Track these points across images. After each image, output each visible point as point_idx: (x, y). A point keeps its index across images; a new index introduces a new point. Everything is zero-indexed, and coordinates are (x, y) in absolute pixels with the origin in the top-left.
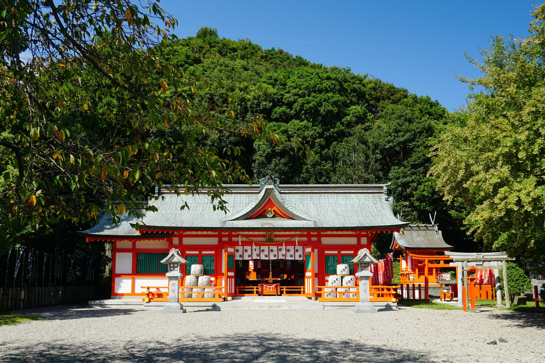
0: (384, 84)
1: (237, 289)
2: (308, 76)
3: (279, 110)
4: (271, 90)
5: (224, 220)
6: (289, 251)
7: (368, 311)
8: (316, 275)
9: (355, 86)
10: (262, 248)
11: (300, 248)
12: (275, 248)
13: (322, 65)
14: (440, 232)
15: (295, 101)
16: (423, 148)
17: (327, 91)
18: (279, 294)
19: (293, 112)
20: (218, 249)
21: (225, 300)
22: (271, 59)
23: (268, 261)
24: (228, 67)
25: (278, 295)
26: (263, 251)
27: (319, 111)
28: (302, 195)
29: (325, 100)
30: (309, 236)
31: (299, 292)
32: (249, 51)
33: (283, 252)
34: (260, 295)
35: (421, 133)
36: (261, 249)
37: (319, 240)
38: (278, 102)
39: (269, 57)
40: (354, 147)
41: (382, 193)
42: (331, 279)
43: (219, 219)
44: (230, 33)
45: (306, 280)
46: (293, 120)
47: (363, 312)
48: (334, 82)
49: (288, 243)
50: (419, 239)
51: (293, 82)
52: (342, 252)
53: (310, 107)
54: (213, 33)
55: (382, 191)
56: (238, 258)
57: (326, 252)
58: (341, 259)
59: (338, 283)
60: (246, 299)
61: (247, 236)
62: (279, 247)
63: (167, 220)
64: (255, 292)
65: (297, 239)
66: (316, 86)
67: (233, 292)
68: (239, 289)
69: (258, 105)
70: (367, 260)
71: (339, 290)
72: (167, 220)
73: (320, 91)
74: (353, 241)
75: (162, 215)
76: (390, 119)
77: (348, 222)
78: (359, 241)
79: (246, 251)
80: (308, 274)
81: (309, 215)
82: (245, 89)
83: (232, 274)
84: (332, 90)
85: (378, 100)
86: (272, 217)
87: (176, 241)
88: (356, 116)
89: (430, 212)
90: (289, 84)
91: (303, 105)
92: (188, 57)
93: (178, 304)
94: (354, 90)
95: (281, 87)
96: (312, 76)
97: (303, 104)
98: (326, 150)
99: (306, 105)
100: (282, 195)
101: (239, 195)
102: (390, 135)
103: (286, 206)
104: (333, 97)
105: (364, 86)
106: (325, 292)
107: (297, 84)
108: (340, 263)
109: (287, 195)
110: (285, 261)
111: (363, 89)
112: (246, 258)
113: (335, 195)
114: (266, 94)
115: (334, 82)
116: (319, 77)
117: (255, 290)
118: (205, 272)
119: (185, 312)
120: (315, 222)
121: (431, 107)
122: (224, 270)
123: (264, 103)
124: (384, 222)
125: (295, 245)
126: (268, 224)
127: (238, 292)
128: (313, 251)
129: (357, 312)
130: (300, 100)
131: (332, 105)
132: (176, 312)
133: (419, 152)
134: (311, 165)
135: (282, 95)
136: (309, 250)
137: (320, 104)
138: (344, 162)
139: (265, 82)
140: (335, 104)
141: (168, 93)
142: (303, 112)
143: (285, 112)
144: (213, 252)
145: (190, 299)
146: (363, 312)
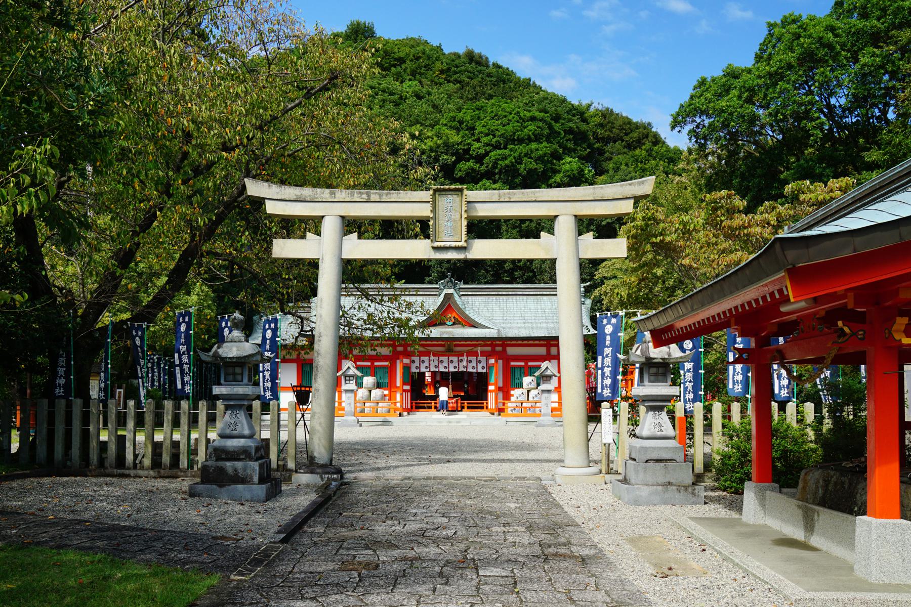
2: (505, 116)
3: (464, 166)
4: (455, 138)
6: (470, 362)
7: (548, 426)
9: (571, 124)
10: (441, 358)
11: (483, 359)
12: (455, 359)
13: (530, 80)
15: (487, 154)
17: (530, 140)
19: (483, 167)
20: (393, 358)
21: (400, 415)
22: (455, 73)
23: (448, 373)
26: (442, 362)
27: (518, 169)
28: (487, 297)
29: (526, 155)
30: (493, 346)
31: (482, 408)
37: (504, 351)
38: (463, 155)
42: (516, 393)
46: (484, 181)
47: (543, 426)
48: (541, 124)
49: (469, 354)
51: (483, 126)
52: (530, 364)
53: (507, 166)
56: (414, 370)
57: (512, 363)
58: (529, 371)
59: (524, 398)
60: (421, 415)
65: (479, 349)
70: (351, 372)
71: (524, 405)
73: (521, 141)
78: (548, 351)
79: (423, 362)
80: (491, 388)
83: (407, 387)
84: (537, 138)
85: (606, 140)
88: (569, 176)
90: (479, 129)
91: (495, 163)
93: (354, 418)
94: (570, 131)
95: (467, 132)
96: (510, 117)
99: (500, 162)
100: (463, 298)
103: (467, 313)
104: (537, 150)
107: (489, 129)
108: (526, 376)
109: (470, 298)
111: (584, 127)
112: (423, 370)
113: (525, 297)
114: (447, 145)
115: (541, 124)
116: (520, 118)
117: (433, 405)
118: (379, 386)
119: (361, 425)
120: (499, 331)
122: (398, 384)
123: (446, 157)
125: (477, 356)
126: (447, 333)
128: (496, 361)
129: (537, 426)
131: (535, 161)
132: (353, 426)
135: (468, 144)
136: (492, 361)
137: (519, 161)
139: (445, 125)
140: (539, 159)
142: (497, 171)
143: (473, 169)
145: (362, 414)
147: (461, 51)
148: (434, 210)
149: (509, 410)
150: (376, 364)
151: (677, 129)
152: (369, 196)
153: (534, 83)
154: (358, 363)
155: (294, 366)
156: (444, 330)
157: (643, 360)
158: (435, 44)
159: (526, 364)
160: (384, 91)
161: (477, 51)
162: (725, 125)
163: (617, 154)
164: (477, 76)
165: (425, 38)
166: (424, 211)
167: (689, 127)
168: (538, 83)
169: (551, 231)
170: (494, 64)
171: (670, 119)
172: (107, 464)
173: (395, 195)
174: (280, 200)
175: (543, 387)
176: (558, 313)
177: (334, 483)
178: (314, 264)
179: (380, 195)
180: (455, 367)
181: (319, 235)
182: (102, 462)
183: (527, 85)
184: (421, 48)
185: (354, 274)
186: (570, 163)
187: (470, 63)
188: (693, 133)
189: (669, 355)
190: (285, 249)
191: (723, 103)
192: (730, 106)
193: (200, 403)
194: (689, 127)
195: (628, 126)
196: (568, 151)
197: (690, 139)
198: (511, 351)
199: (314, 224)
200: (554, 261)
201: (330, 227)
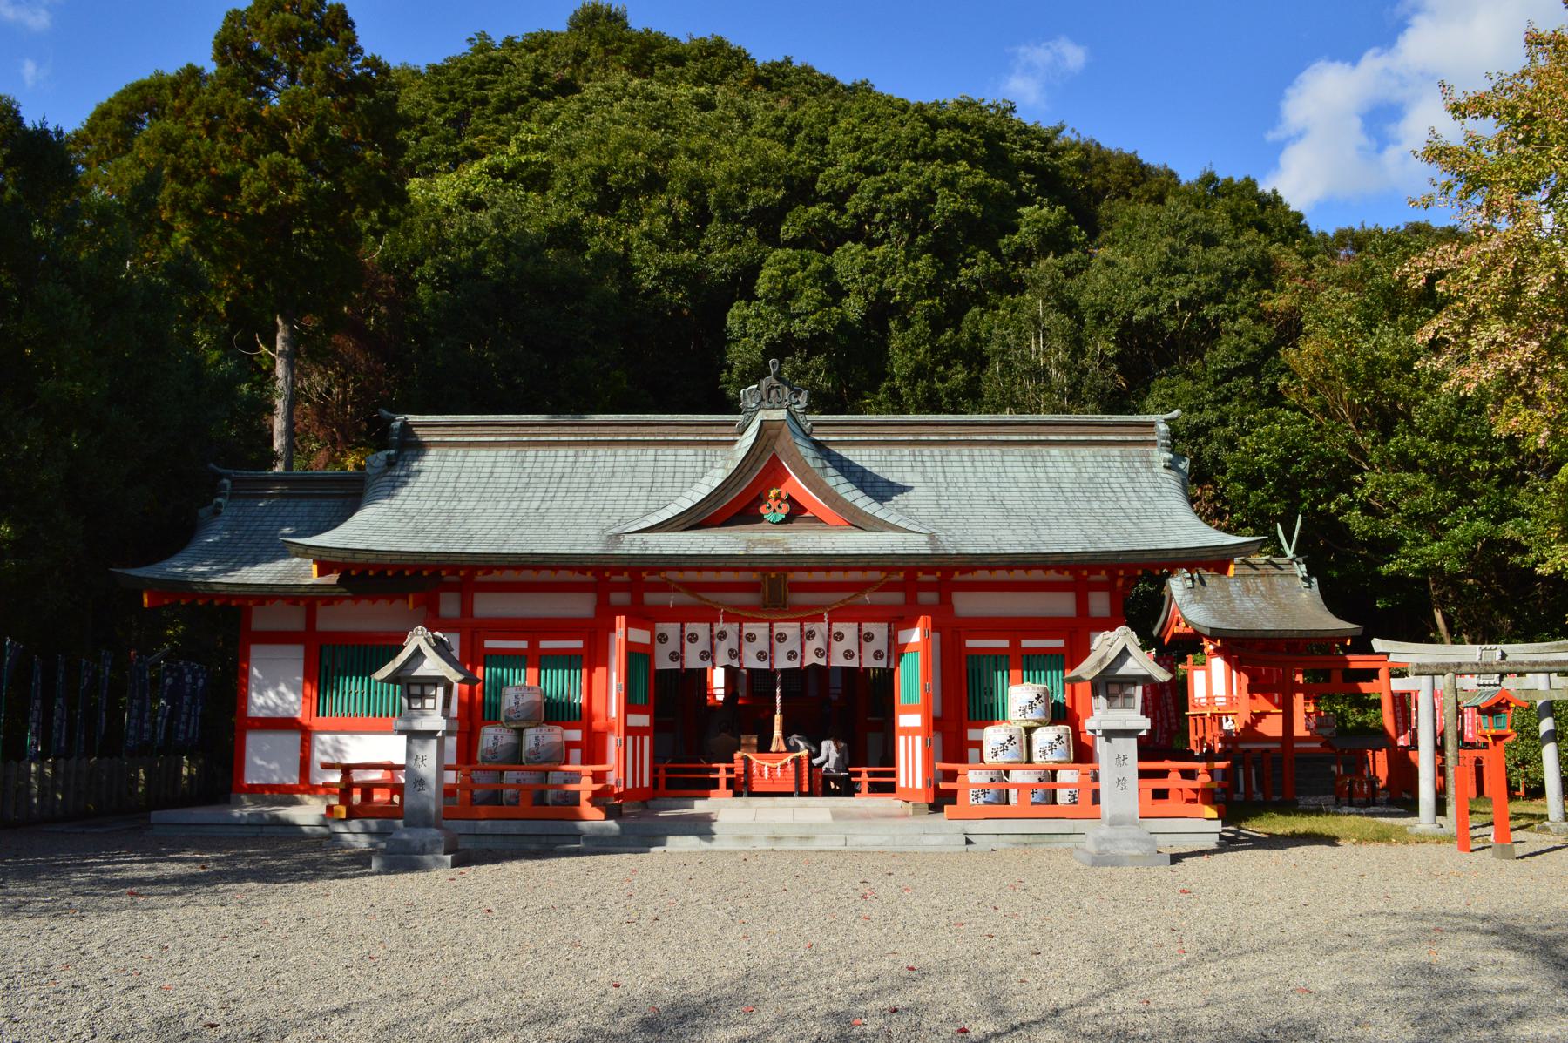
0: (1110, 153)
1: (662, 773)
5: (615, 531)
7: (1135, 860)
10: (748, 628)
12: (791, 629)
14: (1314, 580)
15: (853, 188)
16: (1249, 321)
18: (806, 789)
23: (770, 674)
24: (655, 99)
25: (802, 794)
28: (884, 450)
29: (945, 183)
32: (717, 61)
34: (737, 794)
35: (1242, 275)
36: (745, 631)
37: (946, 602)
38: (801, 190)
39: (774, 78)
40: (1035, 320)
41: (1154, 443)
42: (992, 736)
43: (598, 528)
45: (901, 741)
46: (849, 244)
47: (1116, 862)
50: (1249, 604)
52: (1026, 643)
53: (901, 203)
54: (616, 19)
55: (1150, 438)
56: (663, 663)
57: (970, 643)
61: (692, 587)
62: (808, 626)
63: (417, 531)
64: (722, 783)
66: (916, 141)
67: (646, 783)
68: (667, 771)
69: (742, 198)
70: (1132, 667)
72: (417, 531)
74: (1062, 605)
75: (405, 514)
76: (1145, 237)
77: (1045, 537)
78: (1082, 604)
80: (908, 720)
81: (909, 515)
82: (702, 155)
83: (643, 720)
86: (783, 522)
89: (1280, 519)
92: (538, 78)
98: (949, 333)
101: (669, 451)
102: (1147, 281)
105: (1054, 155)
106: (969, 786)
110: (820, 673)
112: (693, 661)
113: (996, 451)
114: (767, 166)
117: (722, 776)
120: (932, 537)
121: (1263, 206)
124: (1172, 537)
126: (767, 543)
127: (662, 782)
130: (869, 184)
133: (1239, 334)
134: (904, 378)
138: (1008, 365)
141: (618, 373)
144: (578, 644)
146: (1116, 862)
150: (544, 645)
155: (296, 653)
156: (757, 536)
159: (1015, 644)
180: (791, 655)
198: (967, 604)
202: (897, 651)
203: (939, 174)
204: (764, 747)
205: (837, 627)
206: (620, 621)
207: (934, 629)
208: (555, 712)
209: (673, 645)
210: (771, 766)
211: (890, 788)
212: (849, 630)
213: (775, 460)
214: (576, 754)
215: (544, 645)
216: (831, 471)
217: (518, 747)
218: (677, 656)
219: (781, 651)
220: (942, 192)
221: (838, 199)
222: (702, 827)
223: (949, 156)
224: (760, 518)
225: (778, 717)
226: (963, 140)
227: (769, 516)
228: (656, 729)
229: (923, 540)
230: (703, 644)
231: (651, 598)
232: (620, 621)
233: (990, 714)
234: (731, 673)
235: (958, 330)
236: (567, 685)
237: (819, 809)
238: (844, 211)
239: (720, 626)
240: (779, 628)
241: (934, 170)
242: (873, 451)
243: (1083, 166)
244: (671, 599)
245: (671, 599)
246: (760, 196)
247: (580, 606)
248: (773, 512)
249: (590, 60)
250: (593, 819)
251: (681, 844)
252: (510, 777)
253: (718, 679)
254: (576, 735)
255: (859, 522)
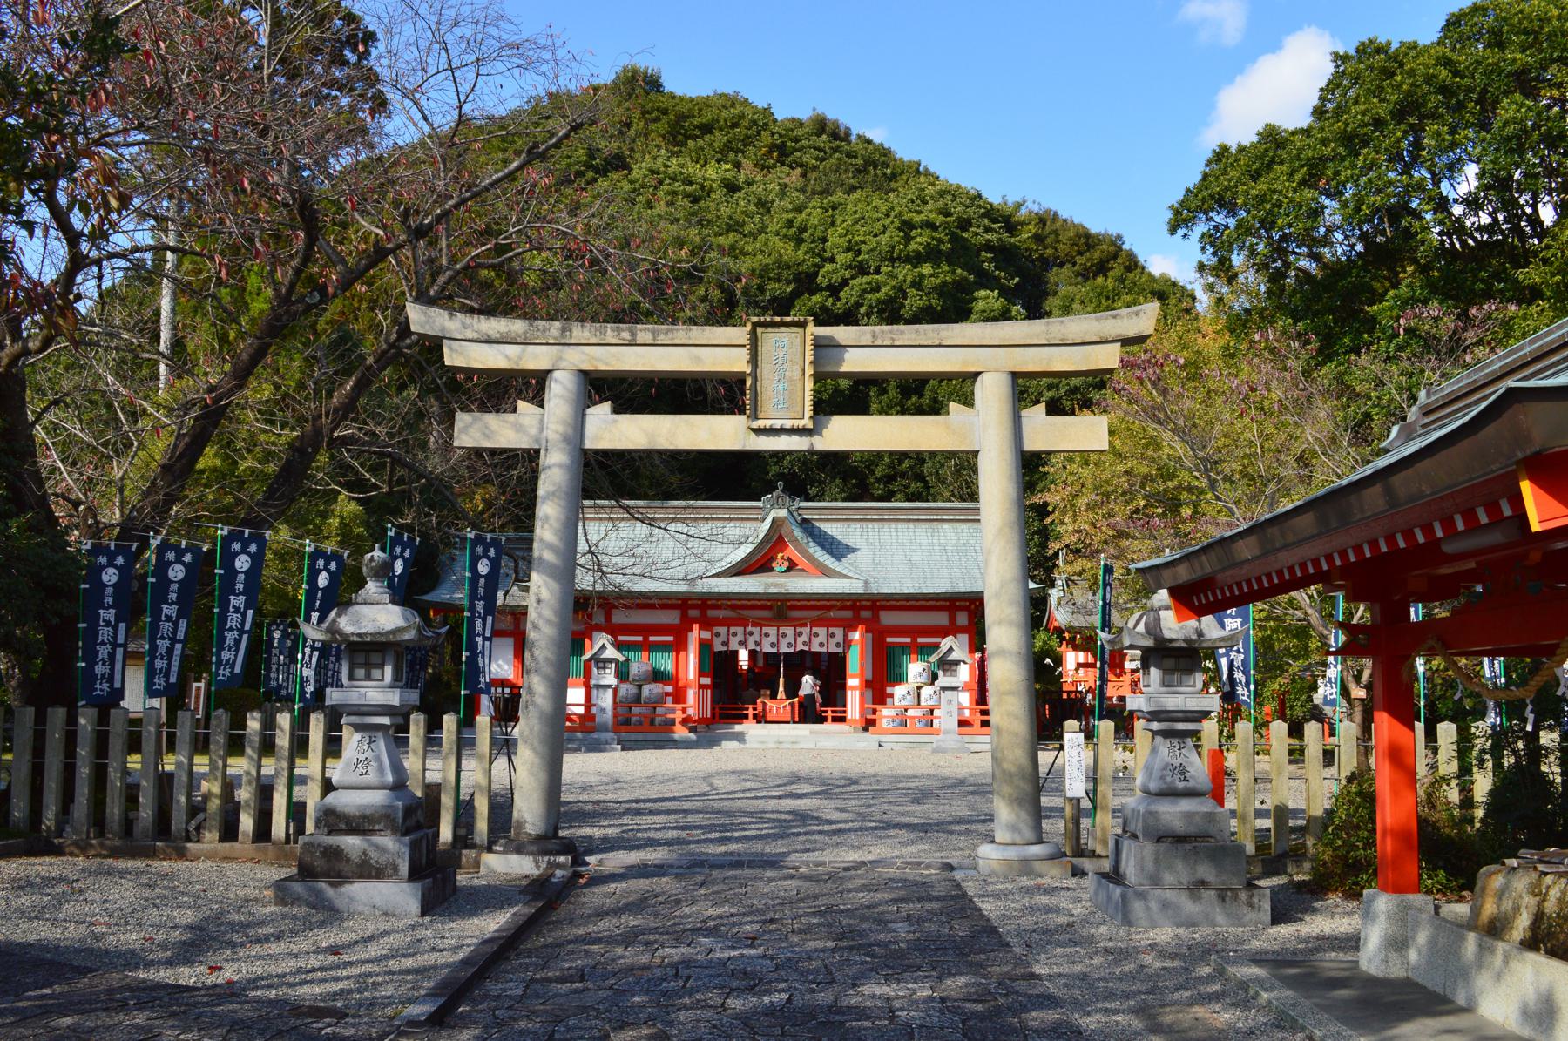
8: (867, 684)
9: (989, 236)
10: (765, 630)
12: (789, 631)
15: (845, 283)
23: (777, 655)
33: (804, 638)
37: (876, 618)
42: (899, 691)
44: (687, 80)
45: (849, 693)
52: (920, 640)
56: (718, 647)
57: (889, 640)
69: (761, 289)
78: (952, 619)
80: (853, 682)
82: (733, 251)
83: (707, 681)
87: (599, 618)
97: (864, 291)
98: (914, 398)
113: (911, 525)
114: (780, 264)
117: (750, 712)
120: (866, 582)
126: (776, 585)
144: (671, 638)
147: (804, 114)
148: (754, 359)
149: (885, 721)
151: (1181, 232)
152: (633, 335)
153: (926, 169)
154: (621, 638)
155: (510, 641)
156: (770, 580)
157: (1149, 643)
158: (761, 103)
160: (673, 179)
161: (831, 116)
162: (1268, 224)
163: (1062, 280)
164: (833, 156)
165: (745, 93)
166: (736, 361)
167: (1201, 228)
168: (932, 169)
169: (968, 401)
170: (859, 136)
171: (1169, 215)
172: (138, 829)
173: (681, 334)
174: (476, 344)
175: (943, 681)
176: (970, 550)
177: (559, 873)
178: (530, 458)
179: (654, 332)
180: (789, 645)
181: (541, 406)
182: (128, 826)
183: (915, 170)
184: (739, 109)
185: (611, 478)
186: (987, 299)
187: (819, 135)
188: (1208, 240)
189: (1200, 634)
190: (477, 430)
191: (1262, 186)
192: (1274, 191)
193: (313, 717)
194: (1201, 228)
195: (1086, 240)
196: (986, 281)
197: (1203, 249)
198: (888, 618)
199: (532, 385)
200: (975, 453)
201: (560, 390)
202: (847, 643)
203: (909, 278)
204: (774, 696)
205: (815, 630)
206: (696, 626)
207: (867, 631)
208: (658, 676)
209: (723, 638)
210: (779, 705)
211: (842, 720)
212: (822, 631)
213: (781, 538)
214: (670, 699)
215: (652, 638)
216: (812, 544)
217: (639, 695)
218: (725, 644)
219: (784, 642)
220: (911, 292)
221: (834, 290)
222: (740, 738)
223: (917, 259)
224: (772, 570)
225: (781, 680)
226: (933, 239)
227: (777, 568)
228: (714, 686)
229: (861, 583)
230: (740, 637)
231: (711, 613)
232: (696, 626)
233: (899, 679)
234: (752, 654)
235: (921, 396)
236: (666, 663)
237: (804, 731)
238: (839, 299)
239: (749, 629)
240: (782, 630)
241: (905, 272)
242: (835, 525)
243: (1038, 238)
244: (722, 614)
245: (722, 614)
246: (775, 288)
247: (672, 618)
248: (780, 566)
249: (633, 131)
250: (681, 732)
251: (727, 745)
252: (635, 710)
253: (743, 656)
254: (670, 689)
255: (826, 572)
